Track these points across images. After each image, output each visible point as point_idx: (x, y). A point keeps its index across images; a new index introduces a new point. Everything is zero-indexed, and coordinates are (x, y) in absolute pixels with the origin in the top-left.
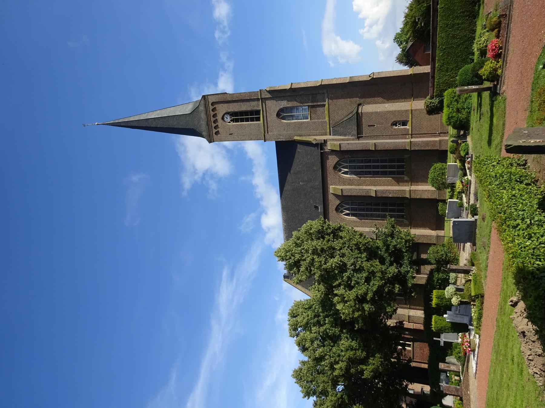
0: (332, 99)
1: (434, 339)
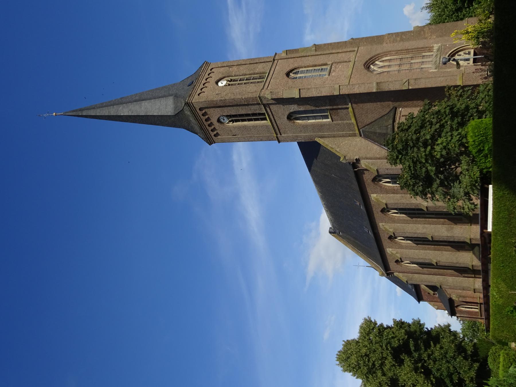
0: (356, 103)
1: (491, 187)
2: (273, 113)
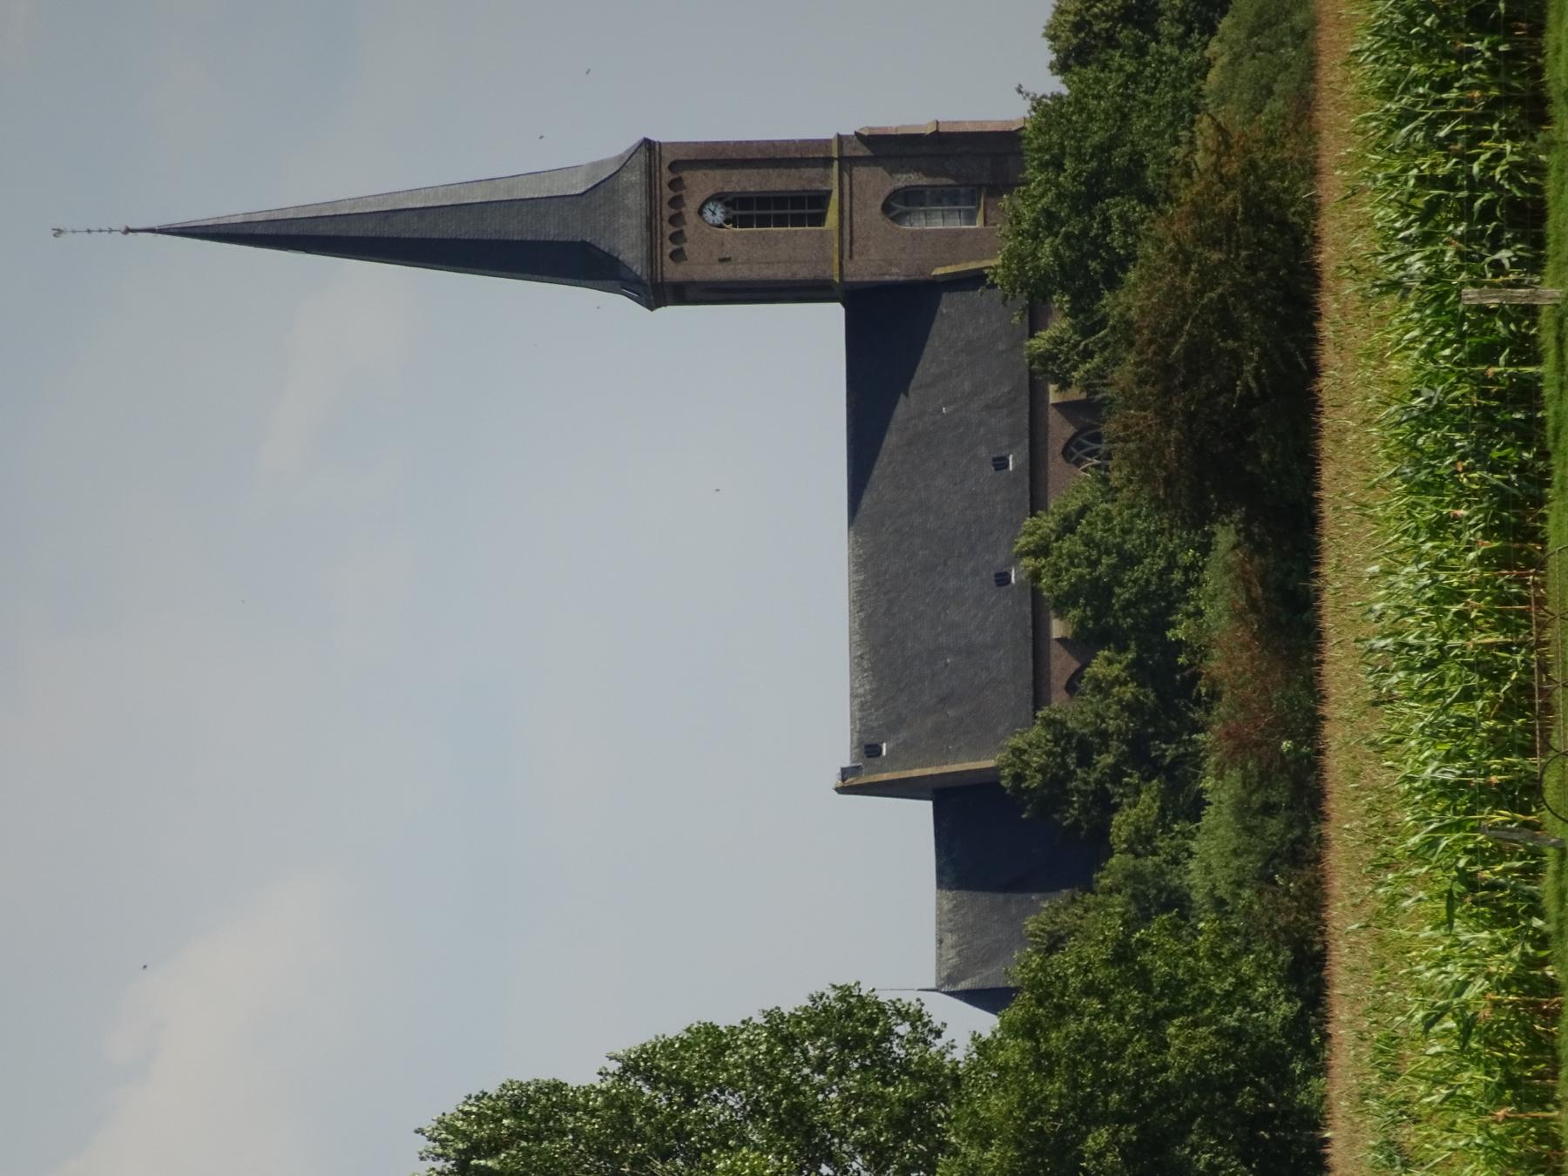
2: (854, 189)
